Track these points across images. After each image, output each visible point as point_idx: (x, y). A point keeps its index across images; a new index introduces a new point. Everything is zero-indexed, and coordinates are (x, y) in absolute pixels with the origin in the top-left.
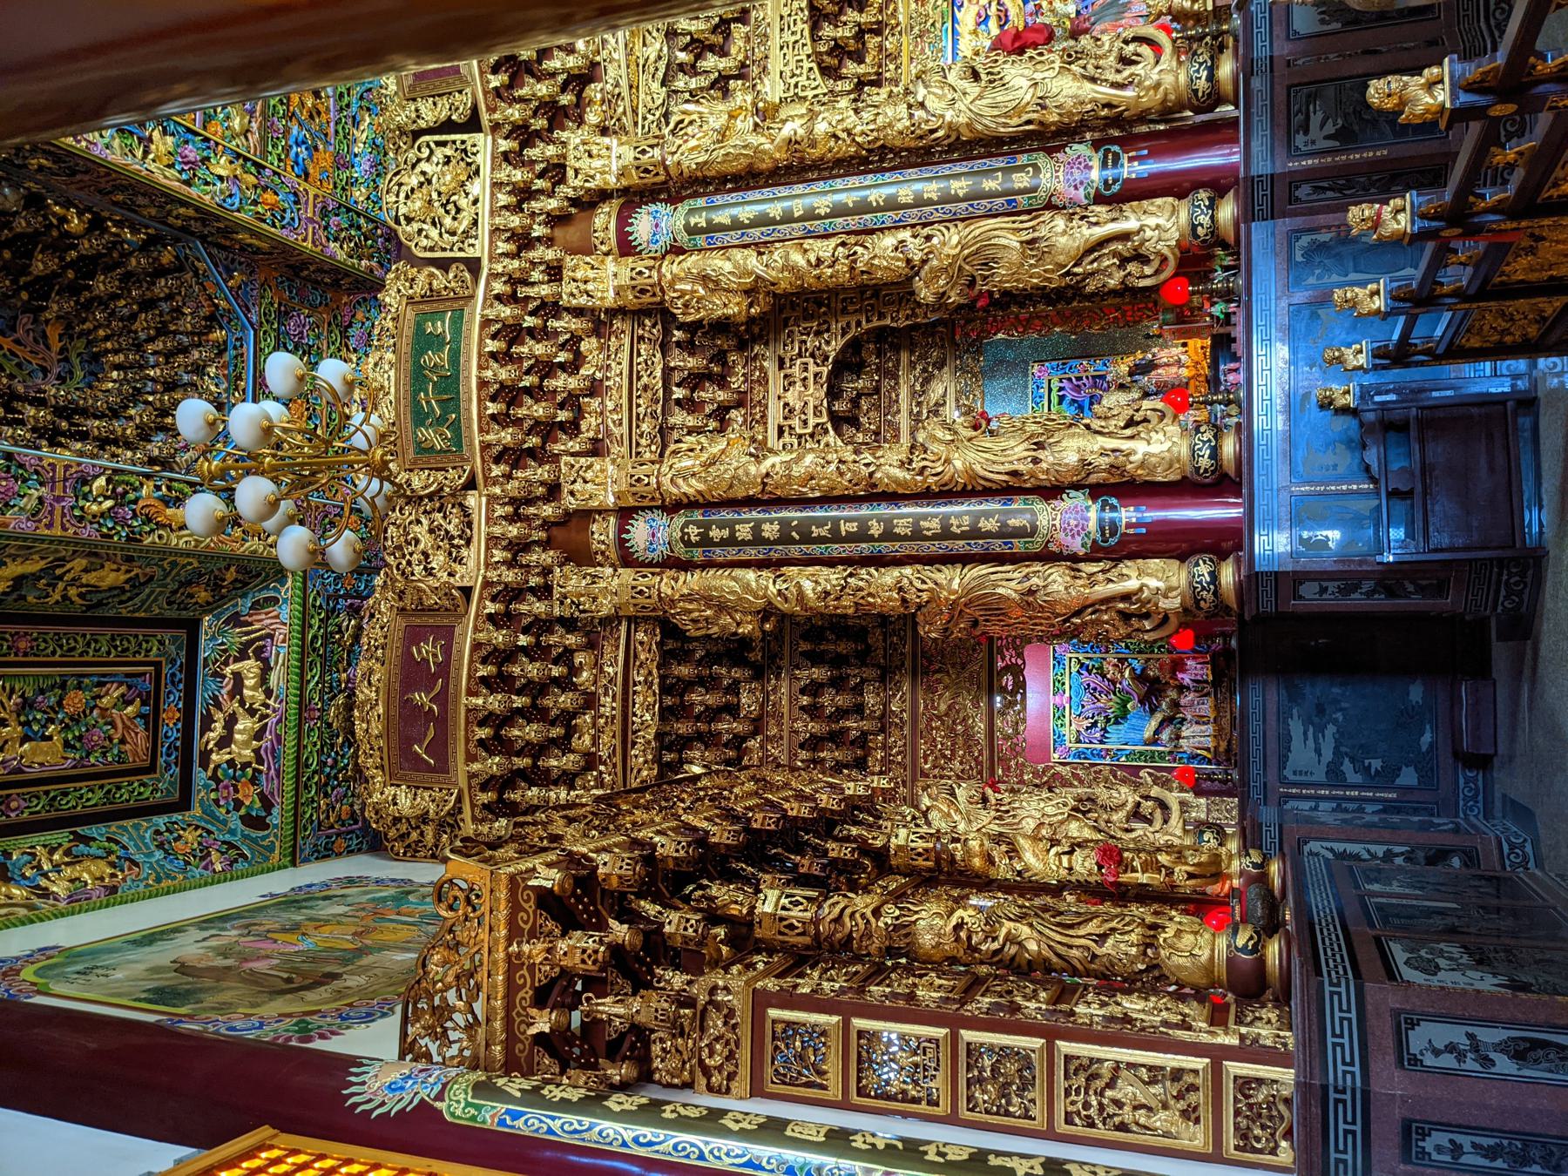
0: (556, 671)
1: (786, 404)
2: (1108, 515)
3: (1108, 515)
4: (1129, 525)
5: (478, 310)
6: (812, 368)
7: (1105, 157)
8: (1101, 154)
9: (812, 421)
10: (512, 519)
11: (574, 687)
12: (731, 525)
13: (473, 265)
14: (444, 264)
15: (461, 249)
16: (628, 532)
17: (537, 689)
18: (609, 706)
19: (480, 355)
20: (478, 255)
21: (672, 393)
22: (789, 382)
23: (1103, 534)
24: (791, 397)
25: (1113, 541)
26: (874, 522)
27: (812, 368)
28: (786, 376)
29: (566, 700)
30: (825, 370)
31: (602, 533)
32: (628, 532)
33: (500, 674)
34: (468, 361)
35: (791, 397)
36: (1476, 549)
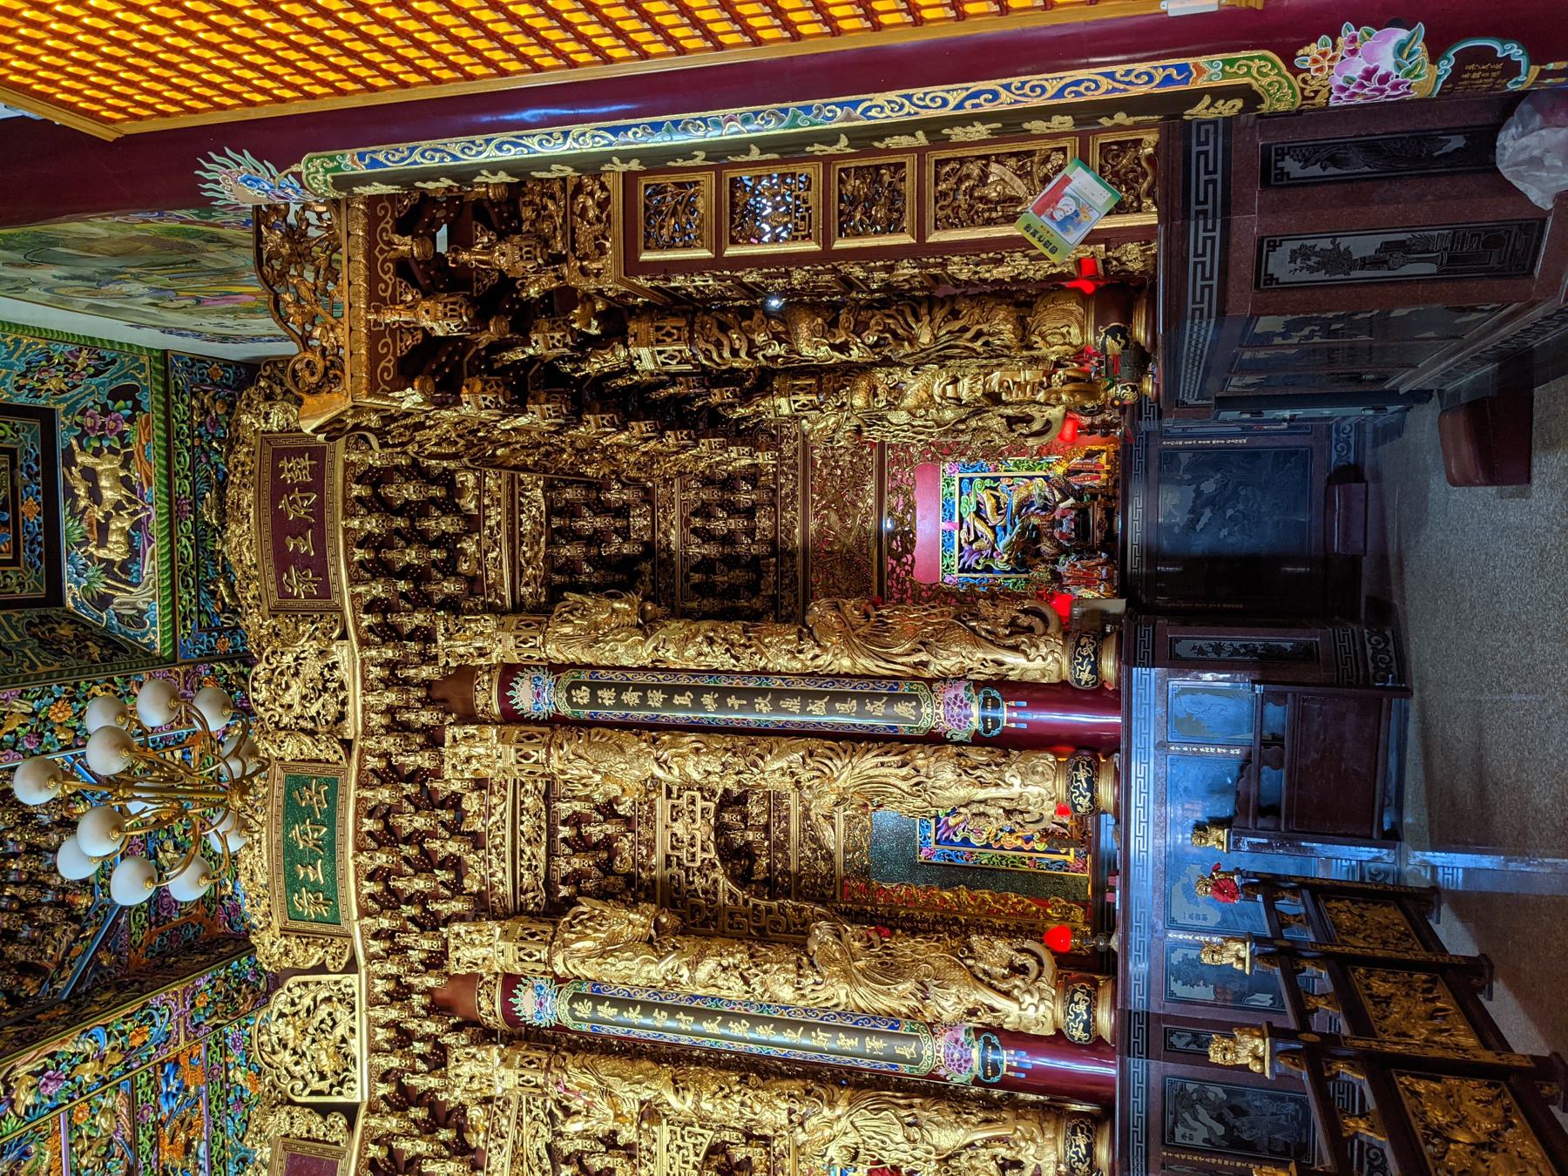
0: (437, 492)
1: (674, 834)
2: (991, 1056)
3: (990, 713)
4: (1010, 1068)
5: (339, 525)
6: (700, 804)
7: (985, 699)
8: (981, 696)
9: (700, 856)
10: (388, 683)
11: (458, 511)
12: (619, 704)
13: (350, 1111)
14: (324, 1110)
15: (340, 1093)
16: (516, 996)
17: (417, 575)
18: (495, 516)
19: (345, 500)
20: (358, 1100)
21: (557, 831)
22: (676, 814)
23: (985, 1073)
24: (679, 828)
25: (996, 732)
26: (765, 710)
27: (700, 804)
28: (673, 806)
29: (447, 525)
30: (712, 805)
31: (486, 698)
32: (516, 996)
33: (378, 560)
34: (345, 844)
35: (679, 828)
36: (1324, 685)
